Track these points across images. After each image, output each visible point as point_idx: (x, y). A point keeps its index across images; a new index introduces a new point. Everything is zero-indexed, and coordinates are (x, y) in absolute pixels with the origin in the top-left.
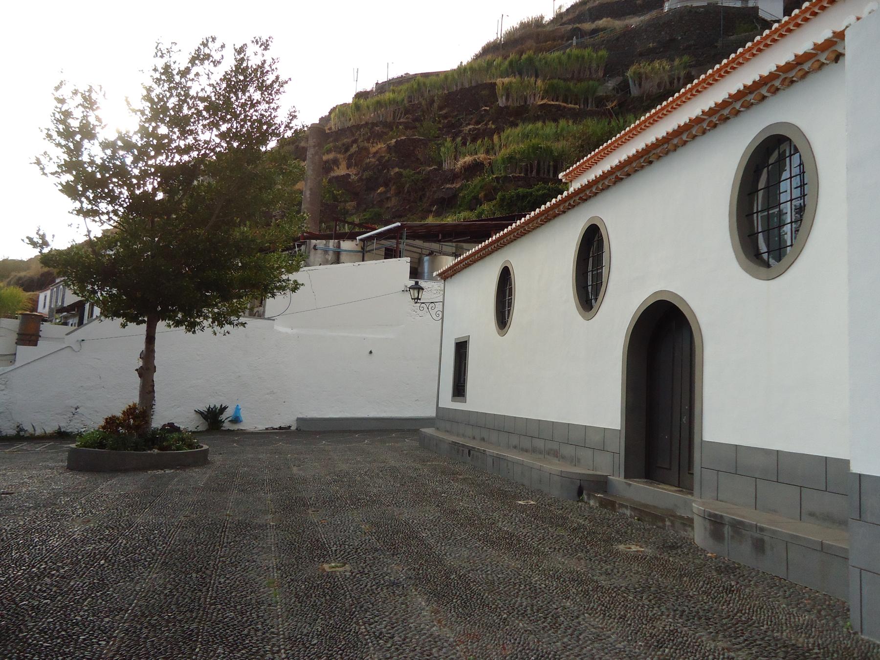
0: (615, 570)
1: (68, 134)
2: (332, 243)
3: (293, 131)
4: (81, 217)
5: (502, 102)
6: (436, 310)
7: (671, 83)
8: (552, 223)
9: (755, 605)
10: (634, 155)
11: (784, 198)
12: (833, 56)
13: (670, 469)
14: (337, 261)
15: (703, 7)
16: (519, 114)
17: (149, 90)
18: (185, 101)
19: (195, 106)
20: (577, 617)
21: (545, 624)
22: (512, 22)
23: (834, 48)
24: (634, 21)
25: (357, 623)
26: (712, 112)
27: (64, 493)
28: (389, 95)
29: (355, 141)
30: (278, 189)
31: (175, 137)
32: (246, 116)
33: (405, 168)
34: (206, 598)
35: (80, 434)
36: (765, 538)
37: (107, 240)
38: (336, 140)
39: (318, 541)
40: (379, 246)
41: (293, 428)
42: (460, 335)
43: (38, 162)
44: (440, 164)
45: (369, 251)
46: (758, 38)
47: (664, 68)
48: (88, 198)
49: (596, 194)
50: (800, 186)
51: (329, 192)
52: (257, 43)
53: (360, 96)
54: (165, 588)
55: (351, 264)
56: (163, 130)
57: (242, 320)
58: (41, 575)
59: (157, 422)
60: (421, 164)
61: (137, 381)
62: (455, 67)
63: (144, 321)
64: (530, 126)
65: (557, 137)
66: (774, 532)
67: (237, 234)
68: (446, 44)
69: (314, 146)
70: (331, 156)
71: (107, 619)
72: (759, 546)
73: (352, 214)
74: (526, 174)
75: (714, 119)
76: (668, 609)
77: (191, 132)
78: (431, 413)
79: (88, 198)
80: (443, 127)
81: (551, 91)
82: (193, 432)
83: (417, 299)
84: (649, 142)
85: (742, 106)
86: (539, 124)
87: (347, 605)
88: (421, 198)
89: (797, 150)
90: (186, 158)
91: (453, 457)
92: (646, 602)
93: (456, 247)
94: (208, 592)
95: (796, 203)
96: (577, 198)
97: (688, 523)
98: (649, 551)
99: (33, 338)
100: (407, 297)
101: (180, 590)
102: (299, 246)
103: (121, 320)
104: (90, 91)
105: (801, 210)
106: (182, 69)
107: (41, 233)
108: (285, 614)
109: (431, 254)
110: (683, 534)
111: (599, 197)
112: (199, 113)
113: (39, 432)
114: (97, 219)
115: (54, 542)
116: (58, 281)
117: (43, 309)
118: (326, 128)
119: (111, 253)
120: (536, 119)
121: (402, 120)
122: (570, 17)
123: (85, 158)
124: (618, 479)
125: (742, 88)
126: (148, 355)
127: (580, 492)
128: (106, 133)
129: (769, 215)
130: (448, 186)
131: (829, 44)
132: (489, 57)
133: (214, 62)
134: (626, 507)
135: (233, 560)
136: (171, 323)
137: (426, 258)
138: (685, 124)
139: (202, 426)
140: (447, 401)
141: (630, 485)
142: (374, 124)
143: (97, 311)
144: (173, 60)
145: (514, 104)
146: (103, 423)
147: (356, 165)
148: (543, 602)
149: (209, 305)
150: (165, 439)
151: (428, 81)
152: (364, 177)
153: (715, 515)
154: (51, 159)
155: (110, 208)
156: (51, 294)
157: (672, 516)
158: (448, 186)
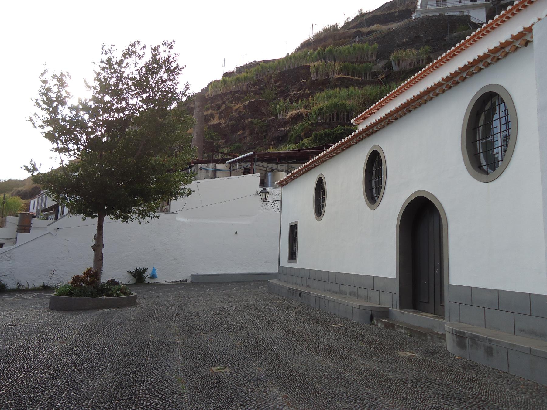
0: (398, 369)
1: (49, 102)
2: (211, 165)
3: (187, 97)
4: (57, 153)
5: (313, 77)
6: (277, 206)
7: (418, 63)
8: (349, 149)
9: (489, 389)
10: (399, 107)
11: (495, 131)
12: (524, 43)
13: (428, 303)
14: (215, 177)
15: (436, 16)
16: (325, 84)
17: (98, 74)
18: (120, 80)
19: (126, 83)
20: (376, 399)
21: (356, 404)
22: (319, 28)
23: (524, 38)
24: (394, 26)
25: (236, 405)
26: (448, 79)
27: (48, 324)
28: (244, 74)
29: (224, 103)
30: (178, 133)
31: (114, 102)
32: (158, 89)
33: (255, 118)
34: (139, 391)
35: (57, 287)
36: (494, 346)
37: (72, 166)
38: (212, 103)
39: (208, 352)
40: (240, 167)
41: (189, 281)
42: (292, 221)
43: (31, 120)
44: (277, 115)
45: (234, 170)
46: (473, 33)
47: (413, 54)
48: (61, 141)
49: (376, 131)
50: (506, 123)
51: (208, 134)
52: (165, 45)
53: (226, 75)
54: (113, 384)
55: (223, 178)
56: (107, 98)
57: (156, 214)
58: (35, 378)
59: (104, 279)
60: (265, 115)
61: (92, 253)
62: (284, 56)
63: (96, 216)
64: (332, 91)
65: (349, 97)
66: (499, 342)
67: (153, 162)
68: (279, 43)
69: (199, 106)
70: (209, 112)
71: (77, 405)
72: (489, 351)
73: (223, 148)
74: (330, 121)
75: (450, 83)
76: (434, 393)
77: (125, 99)
78: (275, 270)
79: (61, 141)
80: (278, 93)
81: (344, 70)
82: (126, 285)
83: (265, 199)
84: (409, 98)
85: (467, 75)
86: (337, 90)
87: (229, 394)
88: (265, 137)
89: (503, 101)
90: (121, 115)
91: (290, 296)
92: (420, 389)
93: (288, 166)
94: (140, 386)
95: (504, 134)
96: (364, 134)
97: (442, 337)
98: (418, 355)
99: (27, 228)
100: (259, 198)
101: (123, 386)
102: (191, 168)
103: (82, 216)
104: (62, 75)
105: (507, 138)
106: (118, 61)
107: (33, 163)
108: (190, 400)
109: (272, 171)
110: (439, 344)
111: (378, 133)
112: (129, 87)
113: (31, 286)
114: (67, 154)
115: (43, 356)
116: (42, 192)
117: (33, 210)
118: (206, 95)
119: (76, 174)
120: (335, 86)
121: (252, 89)
122: (354, 24)
123: (59, 117)
124: (396, 310)
125: (467, 64)
126: (99, 237)
127: (372, 318)
128: (73, 101)
129: (487, 140)
130: (282, 129)
131: (521, 35)
132: (305, 50)
133: (139, 56)
134: (401, 328)
135: (155, 366)
136: (113, 217)
137: (269, 174)
138: (431, 87)
139: (132, 281)
140: (285, 262)
141: (403, 313)
142: (236, 92)
143: (66, 210)
144: (112, 55)
145: (322, 78)
146: (71, 280)
147: (225, 117)
148: (353, 390)
149: (136, 206)
150: (110, 290)
151: (268, 65)
152: (230, 125)
153: (460, 332)
154: (39, 117)
155: (75, 147)
156: (38, 200)
157: (431, 333)
158: (282, 129)
